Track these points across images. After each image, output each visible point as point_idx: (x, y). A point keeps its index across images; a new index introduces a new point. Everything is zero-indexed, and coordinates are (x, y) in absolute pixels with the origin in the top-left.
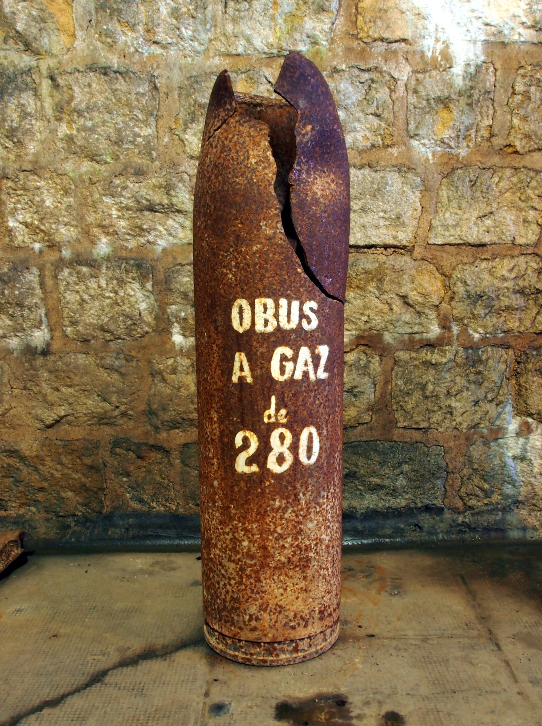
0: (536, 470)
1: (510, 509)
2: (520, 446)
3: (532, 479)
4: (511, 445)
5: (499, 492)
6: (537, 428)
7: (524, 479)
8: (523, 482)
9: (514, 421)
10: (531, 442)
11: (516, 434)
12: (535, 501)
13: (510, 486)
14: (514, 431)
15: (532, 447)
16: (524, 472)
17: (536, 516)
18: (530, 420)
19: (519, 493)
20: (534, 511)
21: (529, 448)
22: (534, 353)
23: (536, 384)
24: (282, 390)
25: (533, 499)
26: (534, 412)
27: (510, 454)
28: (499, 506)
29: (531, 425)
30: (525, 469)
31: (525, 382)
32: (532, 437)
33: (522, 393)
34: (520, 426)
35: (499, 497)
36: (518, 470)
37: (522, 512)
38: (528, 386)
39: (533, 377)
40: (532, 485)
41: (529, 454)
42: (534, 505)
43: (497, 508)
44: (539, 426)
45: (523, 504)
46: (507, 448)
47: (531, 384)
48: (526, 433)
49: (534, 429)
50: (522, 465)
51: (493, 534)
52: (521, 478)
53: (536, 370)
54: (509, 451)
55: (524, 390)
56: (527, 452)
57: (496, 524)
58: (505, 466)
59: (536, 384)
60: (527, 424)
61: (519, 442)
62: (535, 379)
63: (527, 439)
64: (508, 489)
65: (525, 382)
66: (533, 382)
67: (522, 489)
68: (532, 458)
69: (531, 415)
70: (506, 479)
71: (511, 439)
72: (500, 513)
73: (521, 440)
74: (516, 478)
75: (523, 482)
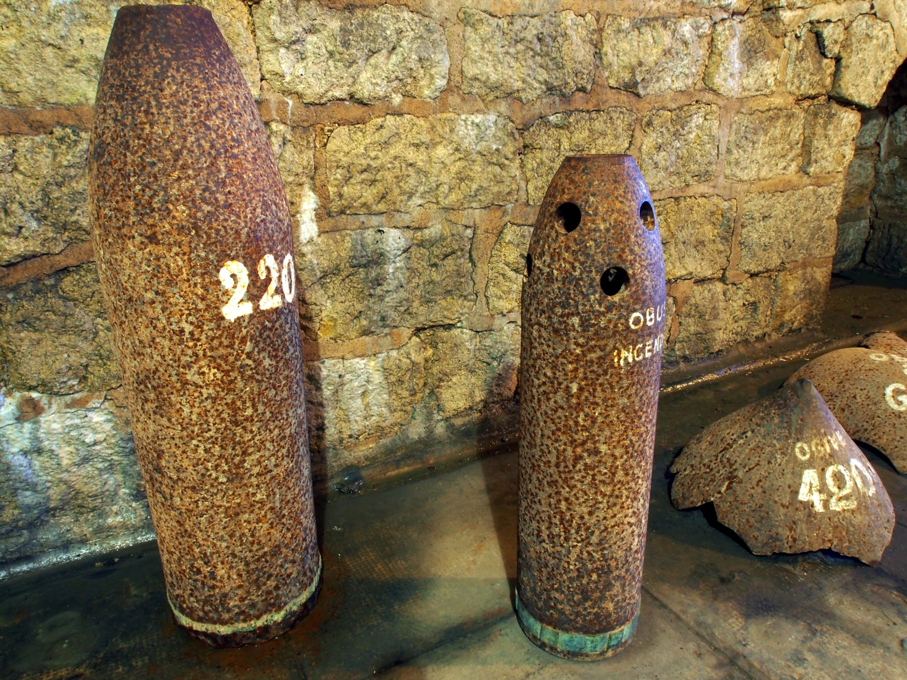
0: (65, 462)
1: (42, 521)
2: (27, 436)
3: (65, 476)
4: (12, 437)
5: (13, 505)
6: (50, 404)
7: (49, 478)
8: (49, 482)
9: (9, 400)
10: (43, 425)
11: (16, 419)
12: (80, 501)
13: (28, 493)
14: (11, 416)
15: (48, 433)
16: (46, 468)
17: (87, 520)
18: (35, 395)
19: (48, 499)
20: (82, 514)
21: (43, 435)
22: (10, 296)
23: (27, 342)
24: (64, 91)
25: (76, 499)
26: (35, 384)
27: (15, 450)
28: (21, 523)
29: (39, 401)
30: (48, 465)
31: (8, 342)
32: (43, 418)
33: (9, 358)
34: (20, 407)
35: (16, 512)
36: (37, 468)
37: (64, 519)
38: (14, 348)
39: (19, 332)
40: (66, 483)
41: (46, 443)
42: (80, 506)
43: (16, 527)
44: (53, 401)
45: (62, 509)
46: (8, 442)
47: (19, 343)
48: (32, 415)
49: (46, 407)
50: (41, 458)
51: (762, 182)
52: (45, 478)
53: (18, 322)
54: (13, 446)
55: (10, 354)
56: (42, 442)
57: (19, 550)
58: (8, 468)
59: (27, 342)
60: (31, 400)
61: (25, 430)
62: (22, 335)
63: (36, 422)
64: (28, 498)
65: (8, 342)
66: (21, 340)
67: (51, 492)
68: (54, 447)
69: (31, 388)
70: (18, 485)
71: (10, 427)
72: (25, 532)
73: (28, 426)
74: (35, 480)
75: (49, 482)
